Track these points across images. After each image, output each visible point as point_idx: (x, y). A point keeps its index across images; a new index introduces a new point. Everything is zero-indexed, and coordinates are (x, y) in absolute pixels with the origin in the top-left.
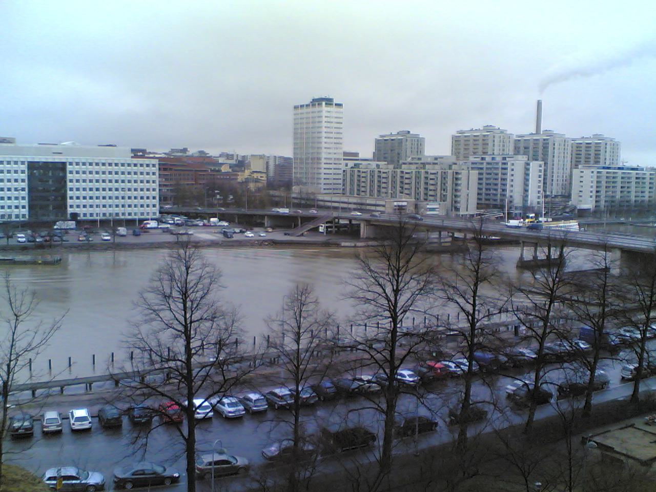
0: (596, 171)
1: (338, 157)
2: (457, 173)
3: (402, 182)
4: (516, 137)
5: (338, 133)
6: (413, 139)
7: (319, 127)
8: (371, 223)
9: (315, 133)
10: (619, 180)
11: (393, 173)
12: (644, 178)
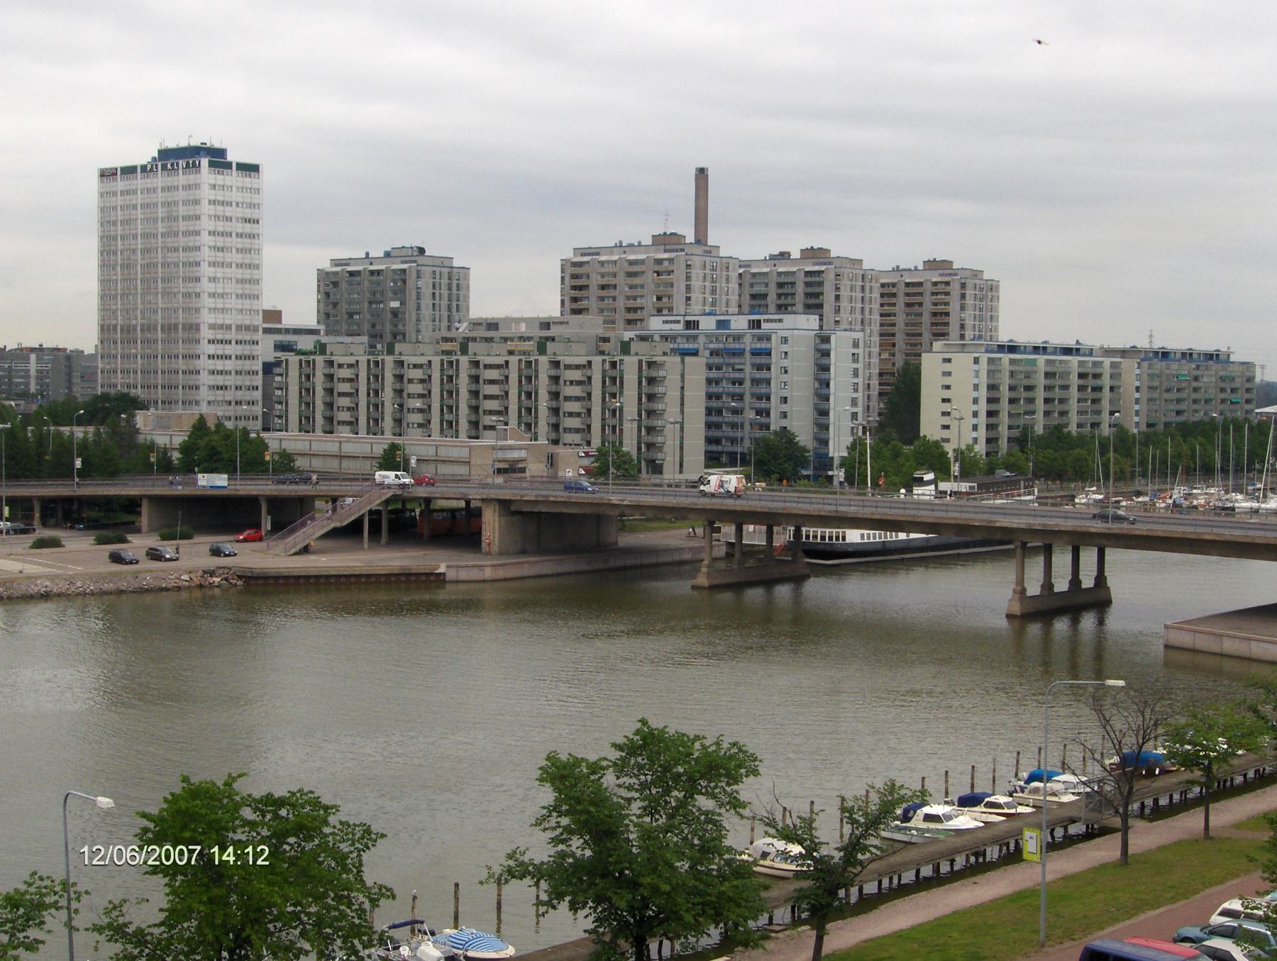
0: (984, 358)
2: (651, 364)
3: (475, 394)
5: (221, 249)
6: (438, 270)
7: (188, 233)
8: (513, 509)
9: (176, 250)
10: (1041, 381)
11: (607, 366)
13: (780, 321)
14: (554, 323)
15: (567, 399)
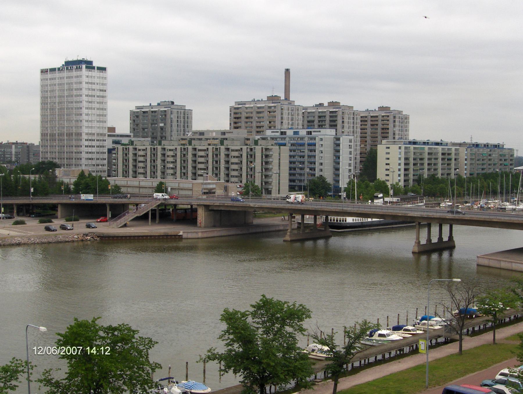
0: (403, 147)
1: (101, 132)
2: (266, 149)
3: (195, 161)
4: (235, 104)
5: (91, 102)
6: (179, 111)
7: (77, 96)
9: (72, 102)
10: (426, 156)
11: (249, 150)
12: (449, 154)
13: (320, 131)
14: (227, 132)
15: (232, 163)
